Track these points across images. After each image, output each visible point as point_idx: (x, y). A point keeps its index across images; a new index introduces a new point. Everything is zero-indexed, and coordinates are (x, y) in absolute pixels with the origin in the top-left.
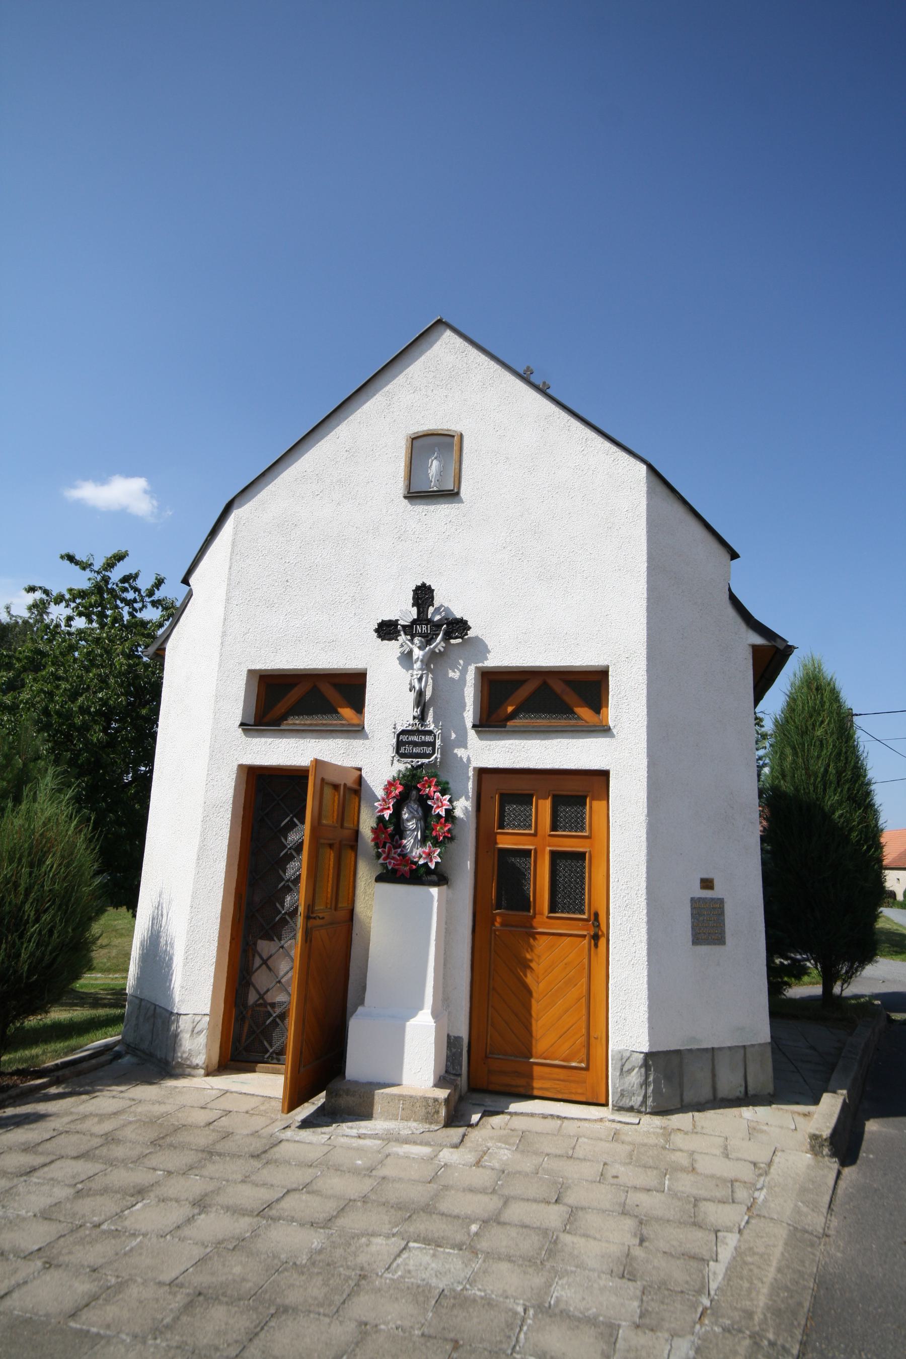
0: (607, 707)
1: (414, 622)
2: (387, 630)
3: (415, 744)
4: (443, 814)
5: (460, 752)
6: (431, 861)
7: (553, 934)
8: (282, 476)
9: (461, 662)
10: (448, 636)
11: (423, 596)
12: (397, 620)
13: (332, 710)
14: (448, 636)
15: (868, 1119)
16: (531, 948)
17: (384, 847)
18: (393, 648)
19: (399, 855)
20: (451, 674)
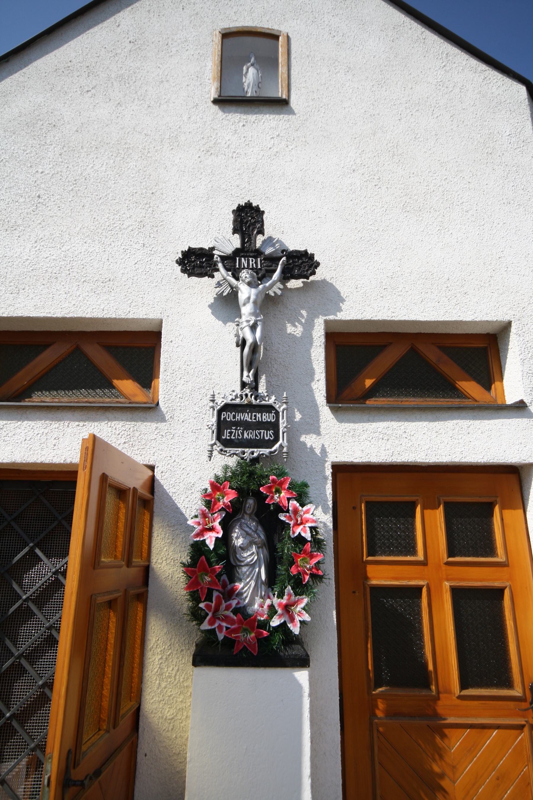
0: (501, 379)
1: (237, 252)
2: (197, 262)
3: (247, 426)
4: (308, 536)
5: (309, 440)
6: (292, 620)
7: (471, 726)
8: (35, 64)
9: (304, 313)
10: (286, 276)
11: (248, 218)
12: (213, 249)
13: (106, 384)
14: (286, 276)
15: (309, 671)
16: (439, 753)
17: (209, 598)
18: (205, 289)
19: (236, 611)
20: (290, 329)
